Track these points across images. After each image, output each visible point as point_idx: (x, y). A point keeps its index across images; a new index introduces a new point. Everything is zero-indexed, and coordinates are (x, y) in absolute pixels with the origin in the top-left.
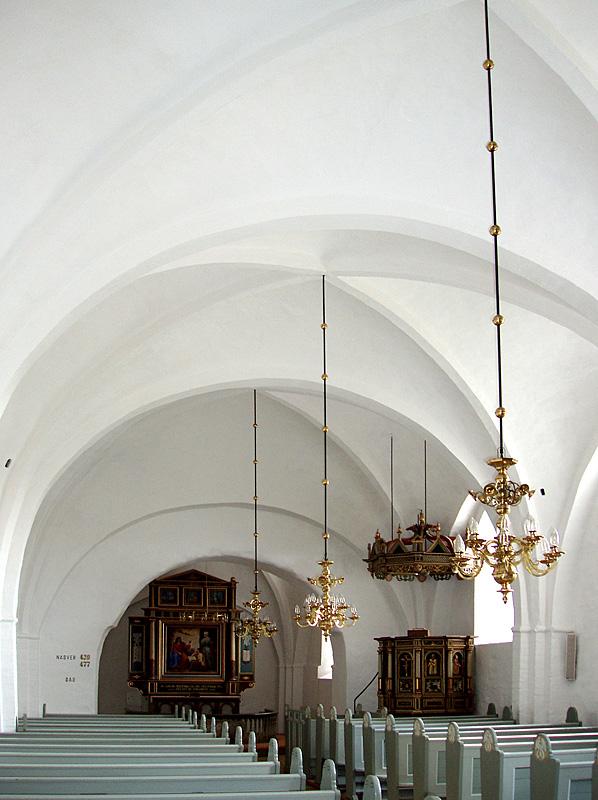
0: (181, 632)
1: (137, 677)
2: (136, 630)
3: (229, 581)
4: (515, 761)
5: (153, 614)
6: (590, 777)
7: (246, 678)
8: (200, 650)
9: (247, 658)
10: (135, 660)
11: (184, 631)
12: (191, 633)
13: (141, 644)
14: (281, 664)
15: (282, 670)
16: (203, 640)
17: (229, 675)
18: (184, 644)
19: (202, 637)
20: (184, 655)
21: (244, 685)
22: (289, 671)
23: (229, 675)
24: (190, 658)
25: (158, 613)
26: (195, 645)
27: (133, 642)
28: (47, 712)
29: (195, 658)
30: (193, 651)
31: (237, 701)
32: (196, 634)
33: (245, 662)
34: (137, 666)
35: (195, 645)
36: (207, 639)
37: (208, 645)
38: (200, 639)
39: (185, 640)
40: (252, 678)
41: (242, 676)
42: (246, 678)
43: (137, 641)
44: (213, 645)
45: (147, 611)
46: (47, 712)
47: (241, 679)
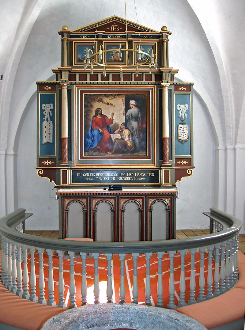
0: (101, 101)
1: (48, 163)
2: (45, 99)
3: (159, 30)
4: (188, 329)
5: (65, 76)
6: (210, 212)
7: (183, 162)
8: (126, 124)
9: (183, 136)
10: (45, 141)
11: (106, 100)
12: (112, 101)
13: (52, 118)
14: (221, 147)
15: (221, 154)
16: (130, 111)
17: (162, 156)
18: (105, 117)
19: (127, 107)
20: (106, 132)
21: (181, 173)
22: (230, 153)
23: (162, 156)
24: (115, 136)
25: (72, 77)
26: (119, 119)
27: (43, 116)
28: (27, 229)
29: (119, 136)
30: (116, 126)
31: (172, 196)
32: (120, 102)
33: (181, 142)
34: (47, 148)
35: (119, 119)
36: (134, 110)
37: (137, 119)
38: (126, 111)
39: (107, 112)
40: (190, 162)
41: (177, 160)
42: (183, 162)
43: (47, 114)
44: (142, 118)
45: (58, 73)
46: (27, 229)
47: (177, 164)
